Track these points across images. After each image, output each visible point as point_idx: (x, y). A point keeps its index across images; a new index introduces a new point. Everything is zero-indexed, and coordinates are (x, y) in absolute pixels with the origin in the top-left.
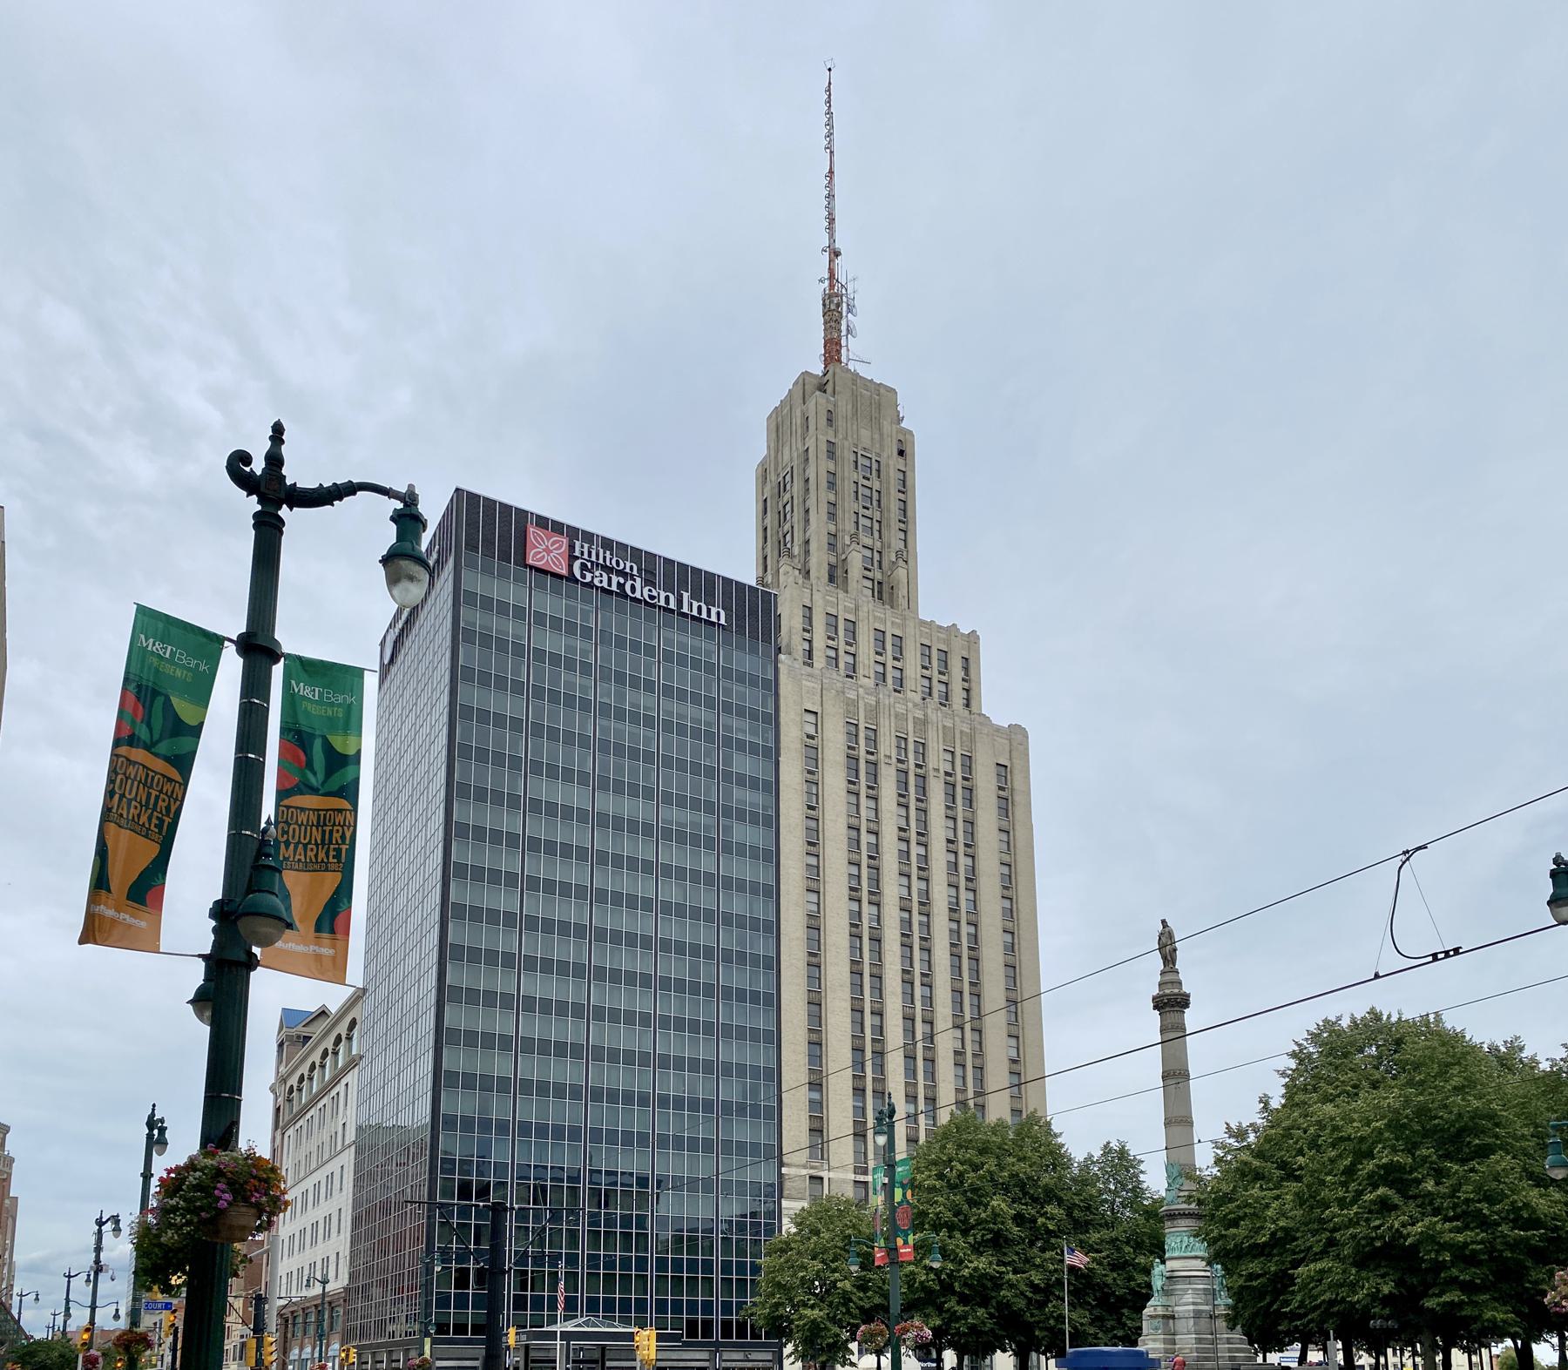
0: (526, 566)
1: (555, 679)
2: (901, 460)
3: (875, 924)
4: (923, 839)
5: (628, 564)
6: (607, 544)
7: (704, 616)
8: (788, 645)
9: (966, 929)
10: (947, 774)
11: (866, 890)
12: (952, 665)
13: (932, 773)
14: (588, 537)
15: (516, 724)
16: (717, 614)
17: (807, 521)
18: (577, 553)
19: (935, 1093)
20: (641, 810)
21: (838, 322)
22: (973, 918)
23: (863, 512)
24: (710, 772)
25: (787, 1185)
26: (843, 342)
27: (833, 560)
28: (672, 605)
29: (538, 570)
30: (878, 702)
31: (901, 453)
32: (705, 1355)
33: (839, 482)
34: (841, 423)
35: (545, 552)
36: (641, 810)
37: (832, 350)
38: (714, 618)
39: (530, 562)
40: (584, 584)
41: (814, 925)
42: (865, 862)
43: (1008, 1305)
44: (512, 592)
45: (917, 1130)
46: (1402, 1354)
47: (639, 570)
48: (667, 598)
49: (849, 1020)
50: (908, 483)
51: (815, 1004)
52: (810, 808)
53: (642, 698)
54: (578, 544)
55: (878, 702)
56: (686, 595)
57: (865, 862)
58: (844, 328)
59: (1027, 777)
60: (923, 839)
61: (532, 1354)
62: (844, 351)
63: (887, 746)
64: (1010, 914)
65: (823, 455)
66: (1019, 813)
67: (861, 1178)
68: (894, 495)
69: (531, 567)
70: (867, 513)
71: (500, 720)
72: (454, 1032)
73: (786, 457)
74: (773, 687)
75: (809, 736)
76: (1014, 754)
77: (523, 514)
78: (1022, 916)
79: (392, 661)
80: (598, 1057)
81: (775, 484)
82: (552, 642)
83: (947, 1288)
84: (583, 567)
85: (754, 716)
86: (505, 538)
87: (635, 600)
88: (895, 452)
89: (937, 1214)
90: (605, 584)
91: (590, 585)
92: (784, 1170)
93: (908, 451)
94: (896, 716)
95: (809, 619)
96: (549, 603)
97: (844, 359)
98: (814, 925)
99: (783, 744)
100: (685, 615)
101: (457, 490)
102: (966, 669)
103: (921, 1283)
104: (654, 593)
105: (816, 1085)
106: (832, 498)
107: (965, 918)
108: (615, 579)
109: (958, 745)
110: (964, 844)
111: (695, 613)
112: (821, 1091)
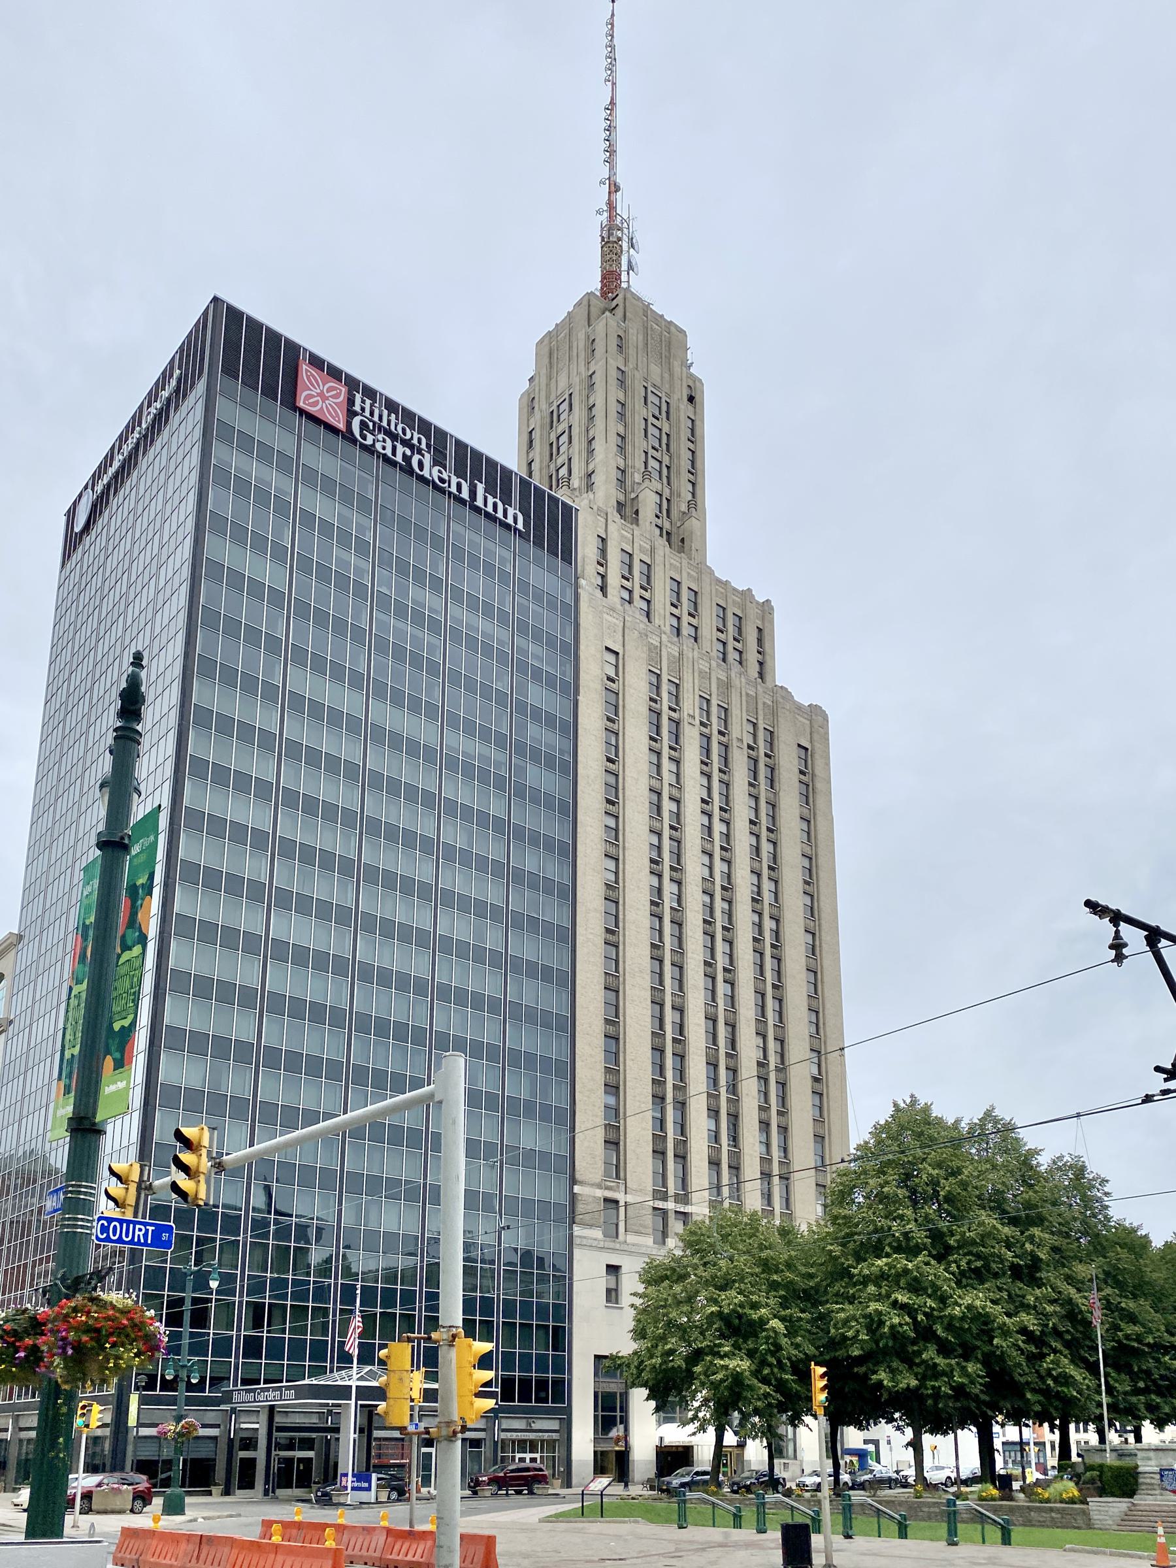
0: (295, 408)
1: (326, 553)
2: (690, 407)
3: (675, 905)
4: (726, 816)
5: (416, 436)
6: (392, 406)
7: (500, 515)
9: (768, 924)
10: (750, 747)
11: (666, 866)
12: (744, 632)
13: (735, 743)
14: (370, 393)
15: (276, 597)
16: (513, 515)
17: (591, 452)
18: (357, 408)
19: (737, 1108)
20: (424, 731)
21: (619, 255)
22: (775, 911)
23: (651, 452)
24: (502, 698)
25: (580, 1207)
27: (622, 498)
28: (465, 495)
29: (311, 418)
30: (681, 654)
31: (691, 399)
33: (628, 414)
34: (632, 352)
35: (317, 396)
36: (424, 731)
38: (510, 521)
39: (301, 404)
40: (364, 448)
41: (613, 894)
42: (666, 833)
43: (1002, 1358)
44: (277, 434)
45: (719, 1150)
46: (1086, 1430)
47: (428, 446)
48: (459, 486)
49: (649, 1013)
50: (698, 432)
51: (613, 988)
52: (609, 760)
53: (428, 597)
54: (358, 397)
55: (681, 654)
56: (480, 488)
57: (666, 833)
58: (624, 267)
59: (828, 764)
60: (726, 816)
61: (278, 1419)
63: (690, 705)
64: (812, 911)
65: (613, 382)
66: (820, 802)
67: (660, 1204)
68: (685, 445)
69: (302, 412)
70: (658, 455)
71: (256, 588)
72: (181, 976)
73: (563, 383)
75: (609, 679)
76: (816, 737)
77: (293, 349)
78: (823, 915)
79: (87, 528)
80: (363, 1028)
81: (547, 414)
82: (320, 506)
83: (925, 1334)
84: (363, 425)
85: (551, 643)
86: (271, 370)
87: (422, 479)
88: (685, 398)
89: (906, 1235)
90: (389, 452)
91: (370, 450)
92: (577, 1189)
93: (697, 399)
94: (700, 672)
95: (603, 551)
96: (320, 458)
98: (613, 894)
99: (582, 682)
100: (477, 510)
101: (216, 300)
103: (892, 1327)
104: (445, 476)
105: (613, 1088)
106: (621, 431)
107: (768, 911)
108: (400, 449)
109: (761, 718)
110: (766, 829)
111: (490, 509)
112: (617, 1095)
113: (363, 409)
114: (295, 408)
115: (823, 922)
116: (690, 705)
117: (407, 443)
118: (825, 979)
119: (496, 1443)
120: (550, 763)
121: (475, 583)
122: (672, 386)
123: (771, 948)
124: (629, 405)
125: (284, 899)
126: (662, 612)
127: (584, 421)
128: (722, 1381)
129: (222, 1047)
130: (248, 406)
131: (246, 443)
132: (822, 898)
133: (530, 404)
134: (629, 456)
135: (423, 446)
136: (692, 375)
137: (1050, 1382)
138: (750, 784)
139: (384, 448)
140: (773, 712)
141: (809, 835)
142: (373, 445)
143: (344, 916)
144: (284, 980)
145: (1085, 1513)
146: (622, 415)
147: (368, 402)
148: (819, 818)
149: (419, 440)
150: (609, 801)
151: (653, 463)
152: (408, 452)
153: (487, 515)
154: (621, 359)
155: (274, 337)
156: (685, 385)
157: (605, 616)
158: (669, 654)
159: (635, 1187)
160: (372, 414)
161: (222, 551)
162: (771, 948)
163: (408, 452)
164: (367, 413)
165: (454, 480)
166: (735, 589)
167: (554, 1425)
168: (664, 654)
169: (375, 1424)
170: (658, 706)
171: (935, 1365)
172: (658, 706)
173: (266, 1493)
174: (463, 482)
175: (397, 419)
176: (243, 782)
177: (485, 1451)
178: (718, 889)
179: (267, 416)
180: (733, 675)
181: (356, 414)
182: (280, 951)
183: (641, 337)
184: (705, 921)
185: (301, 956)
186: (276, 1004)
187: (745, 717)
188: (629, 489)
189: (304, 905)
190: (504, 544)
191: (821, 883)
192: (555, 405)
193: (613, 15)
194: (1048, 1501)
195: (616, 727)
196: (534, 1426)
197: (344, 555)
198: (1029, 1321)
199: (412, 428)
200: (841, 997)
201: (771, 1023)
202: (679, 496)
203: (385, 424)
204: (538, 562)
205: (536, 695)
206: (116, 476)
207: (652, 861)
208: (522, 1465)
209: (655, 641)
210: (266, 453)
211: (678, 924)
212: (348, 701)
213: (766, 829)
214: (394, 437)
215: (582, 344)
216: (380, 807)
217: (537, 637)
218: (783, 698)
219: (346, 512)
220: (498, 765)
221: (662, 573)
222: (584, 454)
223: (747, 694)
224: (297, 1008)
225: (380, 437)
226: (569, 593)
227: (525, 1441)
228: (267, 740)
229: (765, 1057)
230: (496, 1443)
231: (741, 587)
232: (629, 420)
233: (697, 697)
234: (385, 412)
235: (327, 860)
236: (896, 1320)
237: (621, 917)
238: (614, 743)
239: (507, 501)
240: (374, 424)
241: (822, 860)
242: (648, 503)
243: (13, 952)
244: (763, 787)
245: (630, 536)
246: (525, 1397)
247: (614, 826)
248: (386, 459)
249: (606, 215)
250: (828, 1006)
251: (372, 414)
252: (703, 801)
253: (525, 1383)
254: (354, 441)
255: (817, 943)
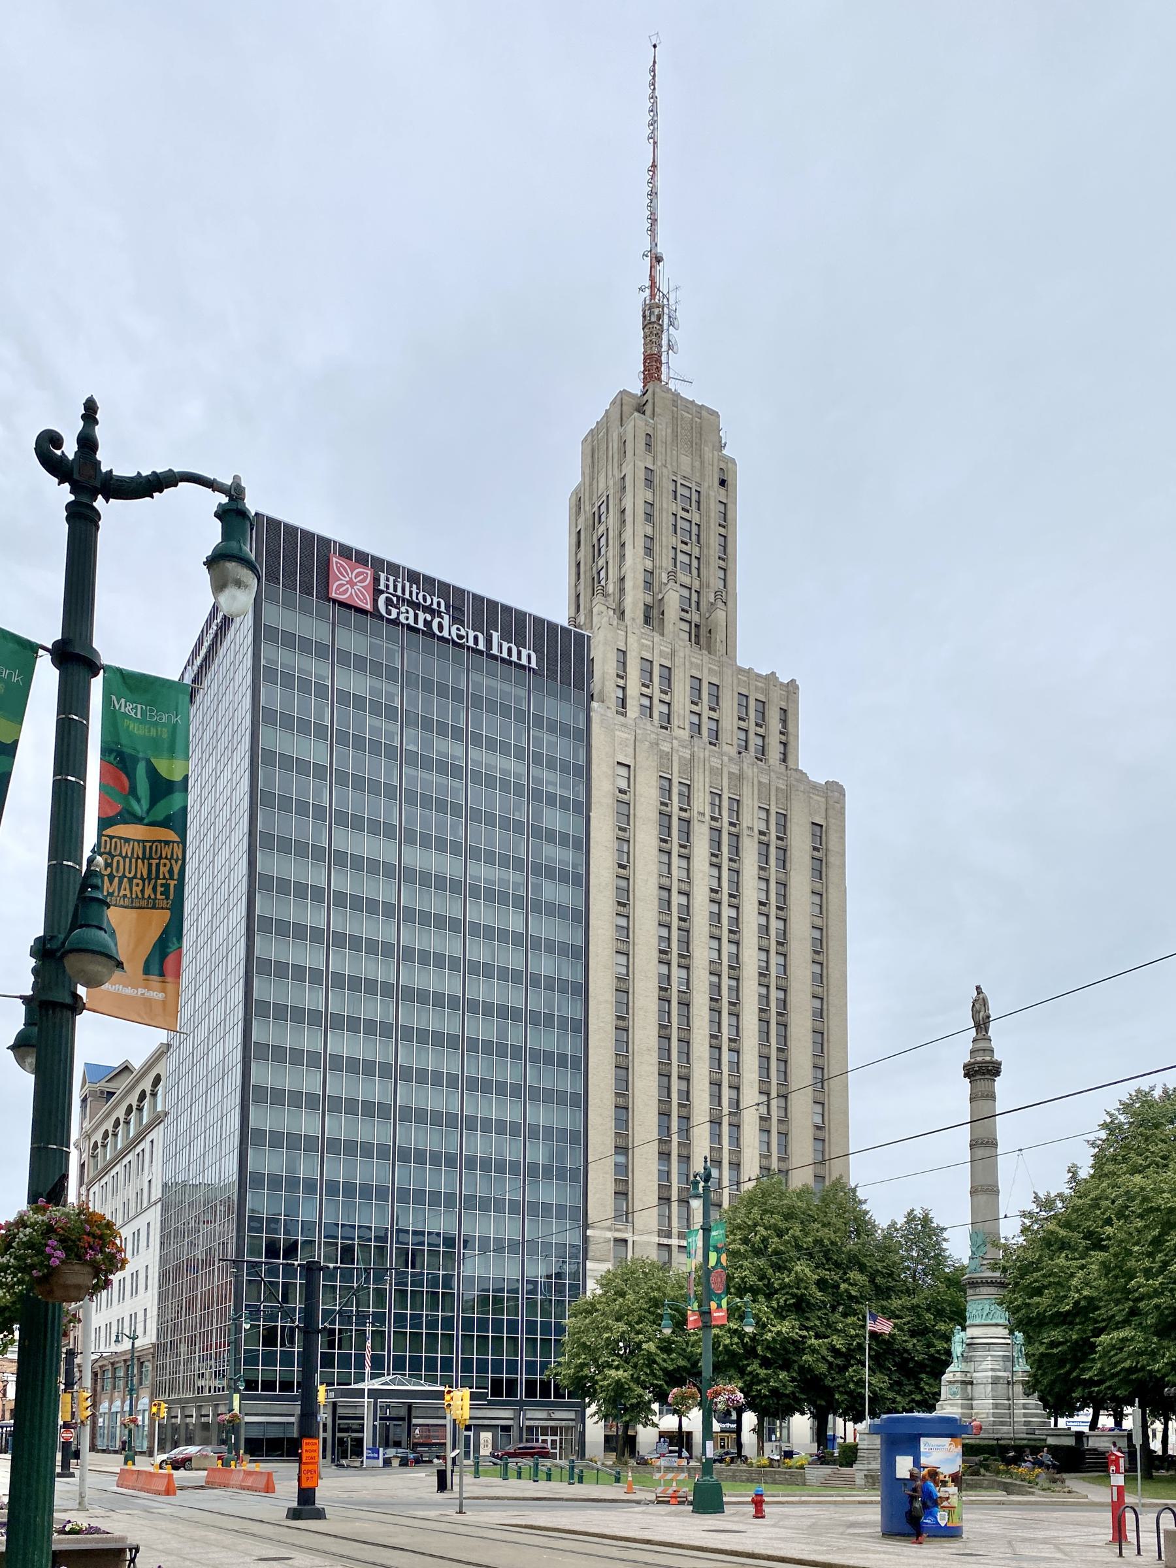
2: (722, 491)
3: (684, 988)
5: (435, 600)
6: (414, 577)
7: (514, 658)
8: (601, 692)
9: (774, 994)
10: (761, 833)
11: (675, 952)
12: (769, 715)
13: (746, 832)
14: (393, 569)
16: (528, 656)
18: (382, 587)
19: (739, 1158)
24: (519, 827)
25: (591, 1248)
26: (664, 359)
27: (649, 600)
28: (481, 646)
29: (342, 604)
30: (692, 755)
31: (723, 483)
32: (508, 1414)
33: (656, 514)
34: (660, 448)
35: (349, 584)
36: (447, 865)
37: (652, 366)
38: (524, 662)
39: (333, 595)
41: (623, 988)
43: (810, 1370)
44: (315, 629)
47: (447, 607)
48: (476, 638)
50: (729, 517)
51: (623, 1068)
54: (383, 576)
56: (496, 636)
61: (340, 1411)
62: (664, 368)
63: (701, 803)
64: (819, 979)
65: (641, 483)
66: (833, 875)
67: (665, 1241)
68: (715, 530)
69: (335, 601)
74: (584, 737)
75: (621, 791)
76: (830, 812)
77: (325, 542)
81: (590, 515)
82: (354, 683)
83: (751, 1352)
84: (389, 602)
85: (565, 768)
86: (307, 570)
87: (442, 639)
90: (411, 622)
91: (395, 622)
92: (589, 1232)
93: (729, 482)
96: (352, 641)
97: (664, 377)
98: (623, 988)
100: (495, 657)
102: (784, 722)
103: (725, 1346)
104: (463, 633)
106: (649, 532)
109: (773, 803)
110: (777, 906)
111: (505, 655)
113: (387, 587)
114: (329, 599)
115: (831, 987)
116: (701, 803)
117: (429, 610)
118: (831, 1039)
119: (521, 1429)
120: (564, 878)
121: (492, 726)
122: (702, 475)
123: (777, 1020)
124: (657, 506)
125: (337, 1022)
126: (682, 712)
127: (617, 525)
128: (609, 1385)
129: (294, 1141)
130: (288, 604)
131: (289, 640)
132: (831, 965)
133: (578, 505)
134: (657, 557)
135: (443, 609)
136: (724, 457)
137: (852, 1386)
138: (761, 868)
139: (407, 619)
140: (787, 795)
141: (821, 909)
142: (398, 618)
143: (386, 1030)
144: (341, 1086)
145: (803, 1476)
146: (649, 517)
147: (392, 578)
148: (831, 890)
149: (439, 604)
150: (619, 903)
151: (682, 558)
152: (429, 618)
153: (503, 660)
154: (649, 459)
155: (308, 536)
156: (716, 469)
157: (617, 733)
158: (680, 758)
159: (641, 1228)
160: (395, 590)
161: (276, 740)
162: (777, 1020)
163: (429, 618)
164: (391, 590)
165: (471, 634)
166: (759, 675)
167: (572, 1415)
168: (675, 758)
169: (413, 1414)
170: (668, 809)
171: (758, 1374)
172: (668, 809)
173: (333, 1461)
174: (480, 635)
175: (418, 588)
176: (300, 931)
177: (514, 1433)
178: (725, 969)
179: (305, 610)
180: (745, 767)
181: (382, 592)
182: (336, 1063)
183: (669, 431)
184: (712, 999)
185: (353, 1065)
186: (335, 1105)
187: (756, 804)
188: (656, 590)
189: (354, 1024)
190: (519, 683)
191: (830, 951)
192: (597, 505)
193: (655, 62)
194: (790, 1468)
195: (627, 835)
196: (553, 1416)
197: (376, 723)
198: (838, 1342)
199: (432, 594)
200: (846, 1053)
201: (774, 1081)
202: (708, 586)
203: (407, 596)
204: (552, 694)
205: (553, 819)
206: (205, 659)
207: (661, 952)
208: (529, 1445)
209: (666, 747)
210: (305, 645)
211: (685, 1004)
212: (382, 849)
213: (777, 906)
214: (415, 606)
215: (616, 446)
216: (413, 937)
217: (551, 765)
218: (797, 780)
219: (377, 684)
220: (517, 885)
221: (682, 675)
222: (617, 559)
223: (760, 782)
224: (351, 1107)
225: (403, 609)
226: (582, 717)
227: (546, 1427)
228: (318, 894)
229: (769, 1113)
230: (521, 1429)
231: (764, 672)
232: (657, 520)
233: (707, 794)
234: (407, 584)
235: (371, 986)
236: (728, 1341)
237: (631, 1004)
238: (625, 850)
239: (521, 644)
240: (398, 597)
241: (833, 930)
242: (673, 600)
243: (164, 1059)
244: (773, 869)
245: (650, 643)
246: (545, 1393)
247: (625, 925)
248: (409, 627)
249: (648, 291)
250: (832, 1062)
251: (395, 590)
252: (712, 890)
253: (545, 1385)
254: (382, 617)
255: (825, 1007)
